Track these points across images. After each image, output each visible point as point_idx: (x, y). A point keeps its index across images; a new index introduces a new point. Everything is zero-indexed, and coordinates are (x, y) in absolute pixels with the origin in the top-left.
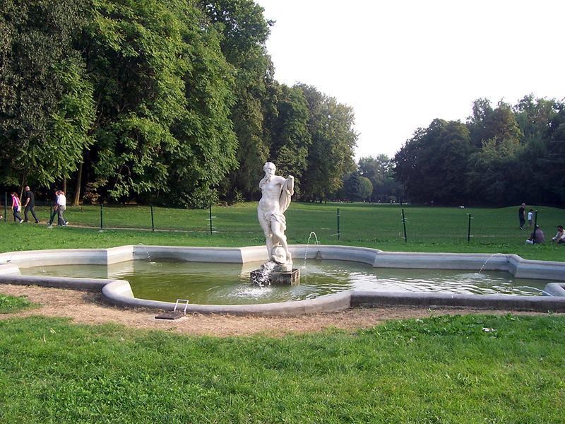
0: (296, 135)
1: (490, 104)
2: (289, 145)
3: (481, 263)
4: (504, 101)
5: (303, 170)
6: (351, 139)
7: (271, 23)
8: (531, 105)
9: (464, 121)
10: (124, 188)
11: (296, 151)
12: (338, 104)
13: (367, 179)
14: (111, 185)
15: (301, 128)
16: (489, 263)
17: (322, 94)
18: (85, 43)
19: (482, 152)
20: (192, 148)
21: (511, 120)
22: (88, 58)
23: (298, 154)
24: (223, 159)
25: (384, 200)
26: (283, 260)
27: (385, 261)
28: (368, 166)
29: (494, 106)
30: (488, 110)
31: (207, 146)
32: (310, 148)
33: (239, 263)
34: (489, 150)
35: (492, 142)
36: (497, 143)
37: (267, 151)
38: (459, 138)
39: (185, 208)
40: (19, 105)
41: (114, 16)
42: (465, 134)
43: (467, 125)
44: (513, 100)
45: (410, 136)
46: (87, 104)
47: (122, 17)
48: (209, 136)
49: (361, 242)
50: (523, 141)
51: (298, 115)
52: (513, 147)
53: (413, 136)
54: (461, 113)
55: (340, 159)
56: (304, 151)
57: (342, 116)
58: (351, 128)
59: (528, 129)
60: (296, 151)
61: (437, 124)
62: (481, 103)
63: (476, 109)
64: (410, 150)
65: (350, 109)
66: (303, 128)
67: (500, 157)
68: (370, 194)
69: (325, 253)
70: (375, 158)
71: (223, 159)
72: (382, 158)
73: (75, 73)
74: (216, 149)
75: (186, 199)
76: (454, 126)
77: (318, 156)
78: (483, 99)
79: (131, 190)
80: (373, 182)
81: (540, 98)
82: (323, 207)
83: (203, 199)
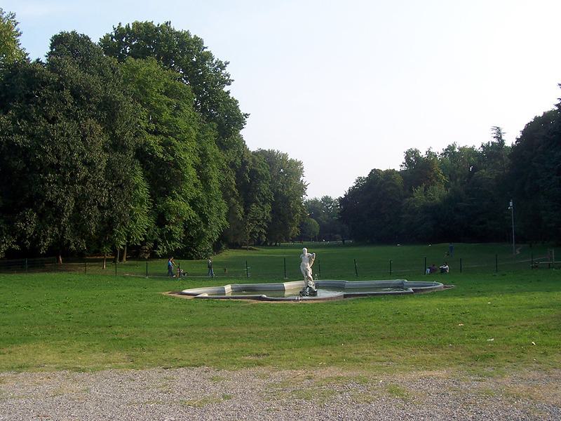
0: (261, 193)
1: (420, 155)
2: (256, 202)
3: (390, 284)
4: (431, 151)
5: (269, 223)
6: (302, 189)
7: (246, 115)
8: (455, 153)
9: (398, 169)
10: (163, 248)
11: (262, 207)
12: (289, 159)
13: (314, 220)
14: (155, 247)
15: (264, 187)
16: (394, 284)
17: (276, 151)
18: (143, 155)
19: (414, 197)
20: (200, 216)
21: (436, 168)
22: (145, 167)
23: (264, 210)
24: (219, 221)
25: (331, 239)
26: (312, 286)
27: (350, 285)
28: (314, 206)
29: (423, 154)
30: (418, 158)
31: (210, 213)
32: (273, 204)
33: (284, 290)
34: (418, 195)
35: (420, 189)
36: (425, 190)
37: (242, 210)
38: (395, 186)
39: (193, 259)
40: (109, 200)
41: (156, 133)
42: (399, 182)
43: (401, 173)
44: (438, 149)
45: (352, 184)
46: (143, 192)
47: (160, 133)
48: (211, 206)
49: (338, 278)
50: (447, 186)
51: (262, 177)
52: (439, 192)
53: (354, 185)
54: (395, 162)
55: (298, 212)
56: (268, 207)
57: (294, 169)
58: (301, 179)
59: (452, 177)
60: (262, 207)
61: (375, 173)
62: (412, 152)
63: (407, 158)
64: (353, 193)
65: (300, 163)
66: (267, 189)
67: (428, 201)
68: (317, 234)
69: (321, 284)
70: (320, 199)
71: (219, 221)
72: (327, 200)
73: (139, 178)
74: (216, 215)
75: (193, 252)
76: (390, 173)
77: (280, 210)
78: (414, 150)
79: (168, 249)
80: (319, 222)
81: (461, 146)
82: (412, 303)
83: (204, 252)
